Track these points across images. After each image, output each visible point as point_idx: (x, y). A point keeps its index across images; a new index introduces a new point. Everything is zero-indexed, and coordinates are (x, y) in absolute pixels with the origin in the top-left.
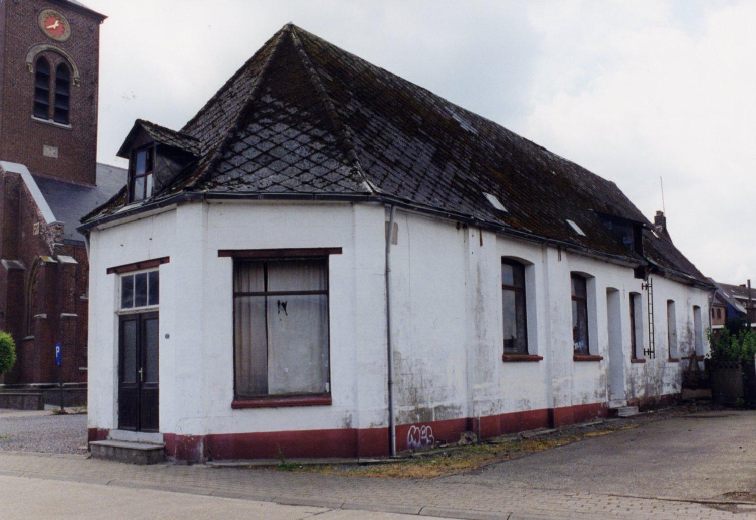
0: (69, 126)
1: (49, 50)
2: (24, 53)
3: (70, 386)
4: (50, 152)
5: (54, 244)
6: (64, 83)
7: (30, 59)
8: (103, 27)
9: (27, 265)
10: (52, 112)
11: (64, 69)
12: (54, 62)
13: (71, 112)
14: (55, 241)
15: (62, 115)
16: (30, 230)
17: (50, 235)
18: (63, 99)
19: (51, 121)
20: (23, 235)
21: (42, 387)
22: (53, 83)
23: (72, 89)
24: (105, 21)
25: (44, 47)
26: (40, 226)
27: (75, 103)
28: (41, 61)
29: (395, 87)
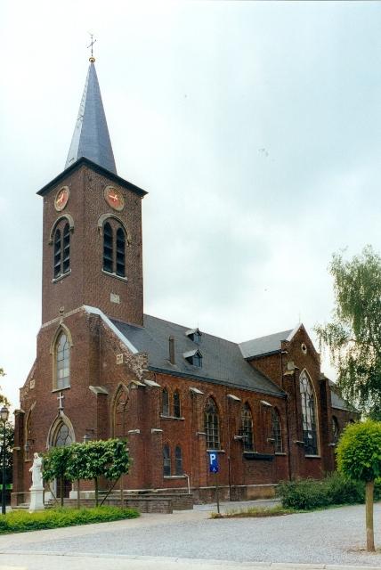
0: (126, 278)
1: (112, 218)
2: (96, 219)
3: (162, 492)
4: (115, 299)
5: (141, 371)
6: (121, 245)
7: (100, 224)
8: (145, 201)
9: (111, 391)
10: (115, 267)
11: (121, 233)
12: (115, 227)
13: (126, 267)
14: (143, 368)
15: (121, 269)
16: (112, 361)
17: (137, 363)
18: (121, 257)
19: (114, 274)
20: (105, 365)
21: (139, 493)
22: (114, 243)
23: (126, 249)
24: (145, 196)
25: (109, 215)
26: (125, 356)
27: (128, 260)
28: (107, 227)
29: (313, 439)
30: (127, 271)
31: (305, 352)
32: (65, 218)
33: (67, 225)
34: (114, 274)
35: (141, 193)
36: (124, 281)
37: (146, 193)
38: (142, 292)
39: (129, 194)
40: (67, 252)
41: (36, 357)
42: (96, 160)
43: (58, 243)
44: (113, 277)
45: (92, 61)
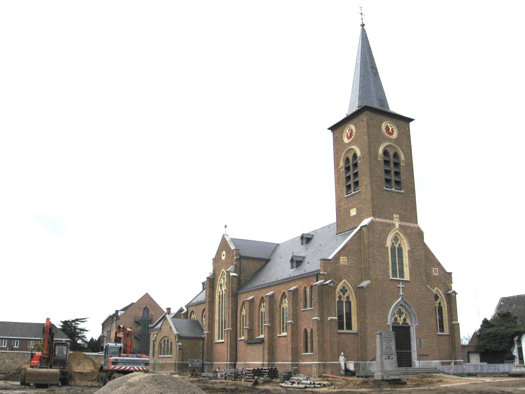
0: (402, 191)
10: (393, 183)
11: (396, 155)
19: (393, 189)
27: (403, 177)
28: (385, 153)
30: (403, 185)
31: (224, 252)
32: (353, 149)
33: (355, 156)
34: (393, 189)
35: (409, 120)
36: (401, 193)
37: (412, 120)
38: (369, 45)
39: (401, 123)
40: (356, 175)
41: (426, 241)
42: (376, 106)
43: (349, 174)
44: (393, 192)
45: (363, 25)
